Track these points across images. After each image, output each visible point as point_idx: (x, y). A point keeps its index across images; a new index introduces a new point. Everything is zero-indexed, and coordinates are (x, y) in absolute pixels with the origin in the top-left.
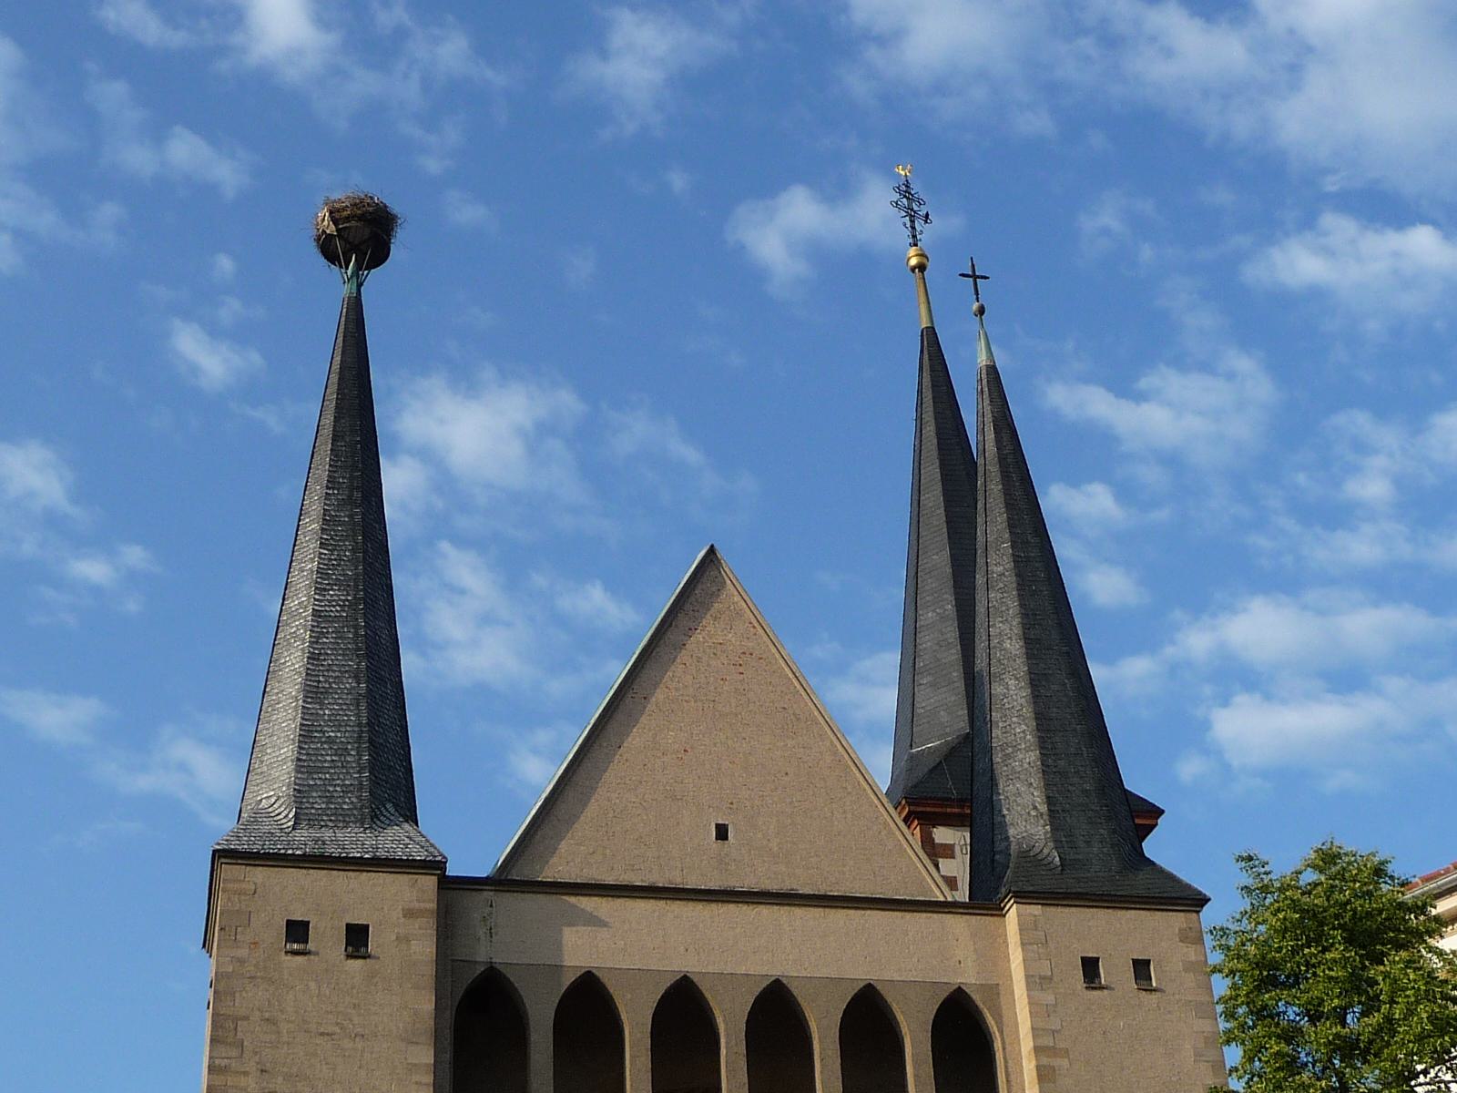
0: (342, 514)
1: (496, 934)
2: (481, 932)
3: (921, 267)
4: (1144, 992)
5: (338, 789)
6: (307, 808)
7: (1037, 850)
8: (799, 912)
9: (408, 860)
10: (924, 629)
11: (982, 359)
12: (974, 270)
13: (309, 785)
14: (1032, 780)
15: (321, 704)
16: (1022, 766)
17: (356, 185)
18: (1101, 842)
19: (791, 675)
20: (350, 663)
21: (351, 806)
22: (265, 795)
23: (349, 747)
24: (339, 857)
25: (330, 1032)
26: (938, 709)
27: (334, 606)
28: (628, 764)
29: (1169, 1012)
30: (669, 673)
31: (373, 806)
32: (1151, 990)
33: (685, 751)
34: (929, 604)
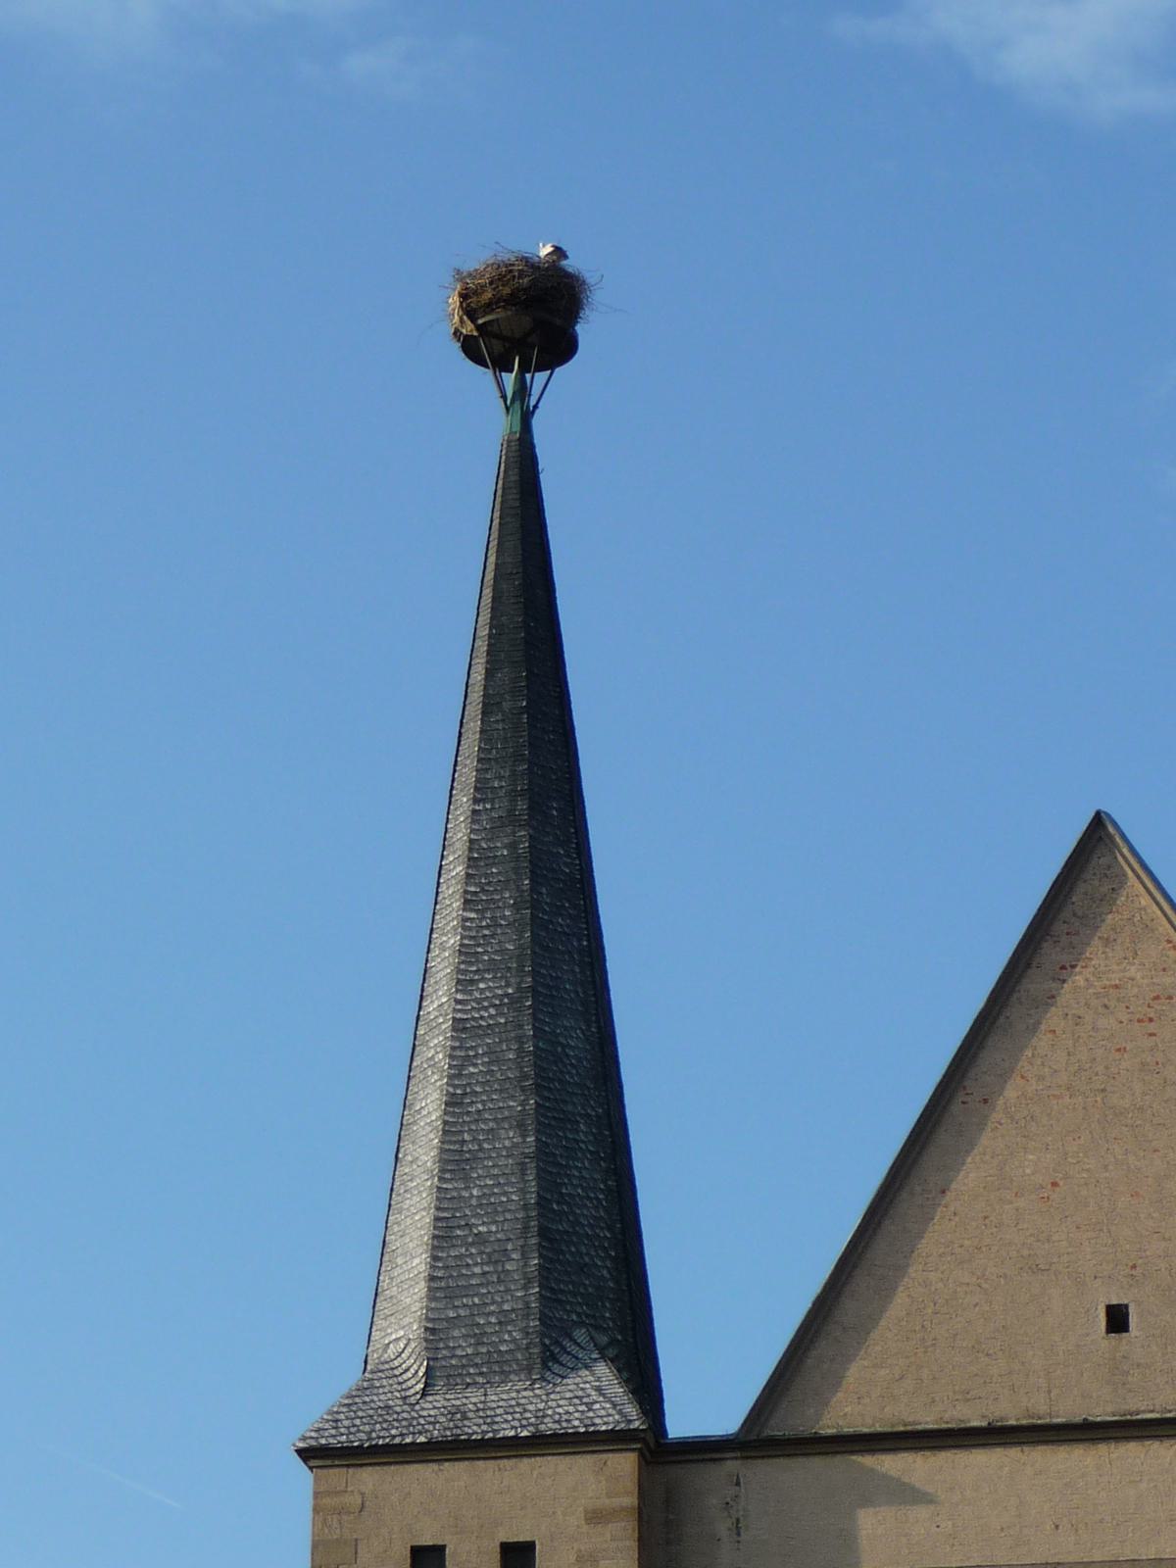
0: (499, 845)
2: (723, 1528)
5: (493, 1320)
6: (444, 1358)
9: (586, 1432)
13: (448, 1320)
15: (466, 1178)
17: (497, 243)
20: (511, 1104)
21: (512, 1346)
22: (394, 1337)
23: (510, 1247)
24: (482, 1439)
27: (486, 1009)
28: (957, 1219)
30: (1029, 1053)
31: (547, 1342)
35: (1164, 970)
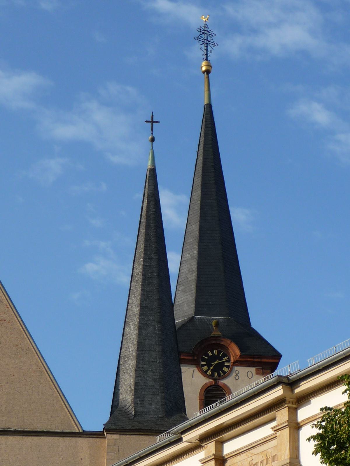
3: (208, 72)
7: (127, 407)
10: (184, 262)
12: (152, 119)
14: (132, 374)
16: (129, 367)
18: (157, 403)
19: (22, 330)
26: (184, 304)
34: (188, 250)
35: (4, 313)
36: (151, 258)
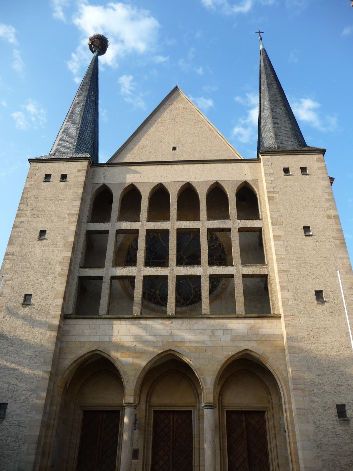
1: (107, 176)
2: (102, 176)
4: (304, 176)
8: (196, 165)
11: (261, 47)
12: (260, 34)
19: (197, 112)
25: (52, 199)
29: (313, 180)
32: (307, 175)
33: (165, 131)
36: (271, 81)
